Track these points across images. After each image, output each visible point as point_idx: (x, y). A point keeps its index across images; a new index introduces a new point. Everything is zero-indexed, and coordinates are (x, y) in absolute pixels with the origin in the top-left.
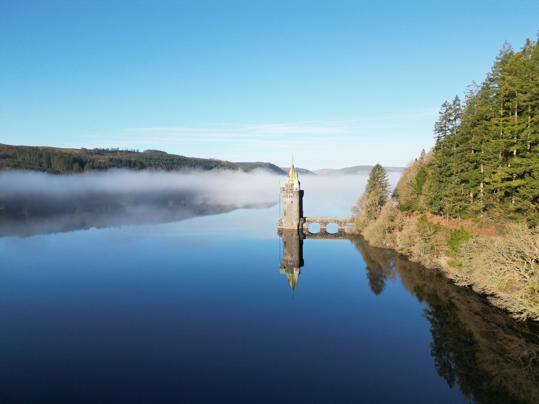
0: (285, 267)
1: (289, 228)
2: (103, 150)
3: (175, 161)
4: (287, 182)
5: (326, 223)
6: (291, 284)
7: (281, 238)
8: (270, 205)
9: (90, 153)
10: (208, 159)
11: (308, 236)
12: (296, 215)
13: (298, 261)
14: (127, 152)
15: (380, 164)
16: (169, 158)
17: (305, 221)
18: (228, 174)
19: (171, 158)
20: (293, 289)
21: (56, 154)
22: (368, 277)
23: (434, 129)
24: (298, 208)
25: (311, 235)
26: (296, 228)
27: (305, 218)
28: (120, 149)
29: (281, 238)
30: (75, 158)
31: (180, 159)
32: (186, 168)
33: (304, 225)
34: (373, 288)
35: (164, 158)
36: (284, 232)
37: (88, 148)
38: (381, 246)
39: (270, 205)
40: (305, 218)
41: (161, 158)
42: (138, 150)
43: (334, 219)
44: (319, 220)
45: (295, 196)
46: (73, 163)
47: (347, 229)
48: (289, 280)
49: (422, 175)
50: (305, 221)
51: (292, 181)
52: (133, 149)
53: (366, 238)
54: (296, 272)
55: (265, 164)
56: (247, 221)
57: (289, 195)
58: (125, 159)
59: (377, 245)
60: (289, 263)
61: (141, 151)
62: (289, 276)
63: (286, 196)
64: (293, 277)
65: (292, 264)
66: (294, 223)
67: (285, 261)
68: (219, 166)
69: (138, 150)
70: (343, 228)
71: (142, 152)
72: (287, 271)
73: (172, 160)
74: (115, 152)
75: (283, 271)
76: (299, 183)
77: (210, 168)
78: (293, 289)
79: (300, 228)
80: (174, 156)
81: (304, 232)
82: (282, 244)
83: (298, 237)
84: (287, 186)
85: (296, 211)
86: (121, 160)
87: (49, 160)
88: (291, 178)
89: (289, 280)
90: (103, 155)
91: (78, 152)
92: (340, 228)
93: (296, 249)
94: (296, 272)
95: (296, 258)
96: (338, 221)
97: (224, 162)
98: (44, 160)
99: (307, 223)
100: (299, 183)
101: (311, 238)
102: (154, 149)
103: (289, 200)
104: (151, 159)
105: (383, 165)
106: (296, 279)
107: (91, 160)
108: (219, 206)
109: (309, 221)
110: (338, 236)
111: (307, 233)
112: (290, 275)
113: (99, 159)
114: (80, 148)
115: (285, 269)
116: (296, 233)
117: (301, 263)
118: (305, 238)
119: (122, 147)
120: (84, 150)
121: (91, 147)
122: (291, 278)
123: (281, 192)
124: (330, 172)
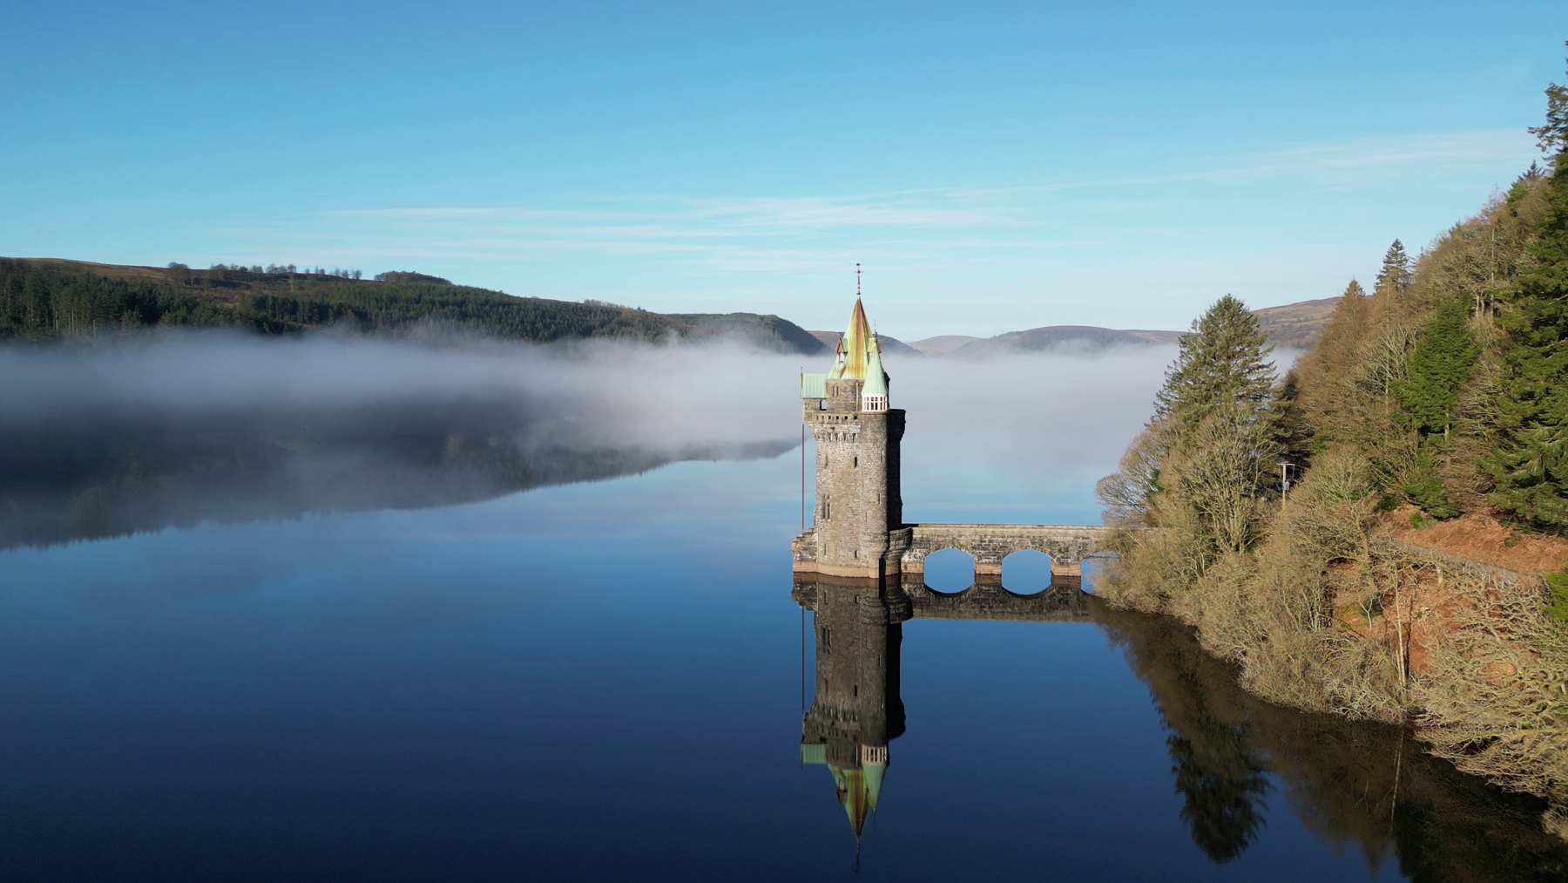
0: (823, 740)
1: (844, 572)
2: (243, 270)
3: (470, 308)
4: (833, 375)
5: (999, 552)
6: (849, 808)
7: (809, 615)
8: (775, 449)
9: (197, 281)
10: (582, 302)
11: (924, 604)
12: (874, 519)
13: (881, 723)
14: (321, 278)
15: (1238, 296)
16: (451, 298)
17: (909, 542)
18: (674, 357)
19: (459, 298)
20: (859, 834)
21: (65, 282)
22: (1180, 786)
23: (1544, 122)
24: (883, 488)
25: (939, 600)
26: (874, 574)
27: (910, 528)
28: (300, 270)
29: (809, 615)
30: (134, 295)
31: (487, 302)
32: (483, 329)
33: (906, 558)
34: (1202, 834)
35: (438, 299)
36: (819, 589)
37: (194, 265)
38: (1310, 700)
39: (775, 449)
40: (910, 528)
41: (426, 297)
42: (358, 274)
43: (1037, 532)
44: (969, 534)
45: (869, 434)
46: (120, 311)
47: (1094, 578)
48: (840, 793)
49: (1444, 347)
50: (909, 542)
51: (857, 369)
52: (342, 270)
53: (1213, 639)
54: (872, 766)
55: (762, 318)
56: (725, 487)
57: (841, 429)
58: (306, 299)
59: (1288, 694)
60: (842, 725)
61: (368, 275)
62: (840, 775)
63: (831, 436)
64: (858, 779)
65: (854, 726)
66: (863, 552)
67: (823, 710)
68: (614, 325)
69: (358, 274)
70: (1074, 571)
71: (371, 278)
72: (832, 755)
73: (460, 304)
74: (281, 277)
75: (814, 755)
76: (886, 379)
77: (587, 332)
78: (859, 834)
79: (888, 571)
80: (468, 291)
81: (906, 587)
82: (812, 638)
83: (878, 611)
84: (834, 389)
85: (874, 498)
86: (295, 304)
87: (44, 299)
88: (850, 360)
89: (840, 793)
90: (235, 286)
91: (160, 276)
92: (1060, 571)
93: (874, 662)
94: (872, 766)
95: (871, 701)
96: (1052, 543)
97: (630, 311)
98: (28, 300)
99: (918, 552)
100: (886, 379)
101: (937, 613)
102: (409, 271)
103: (842, 452)
104: (394, 300)
105: (1253, 302)
106: (874, 793)
107: (185, 303)
108: (613, 453)
109: (925, 543)
110: (1051, 608)
111: (918, 594)
112: (847, 772)
113: (225, 300)
114: (164, 264)
115: (823, 747)
116: (874, 593)
117: (893, 722)
118: (910, 615)
119: (306, 261)
120: (179, 271)
121: (200, 261)
122: (851, 786)
123: (809, 417)
124: (968, 348)
